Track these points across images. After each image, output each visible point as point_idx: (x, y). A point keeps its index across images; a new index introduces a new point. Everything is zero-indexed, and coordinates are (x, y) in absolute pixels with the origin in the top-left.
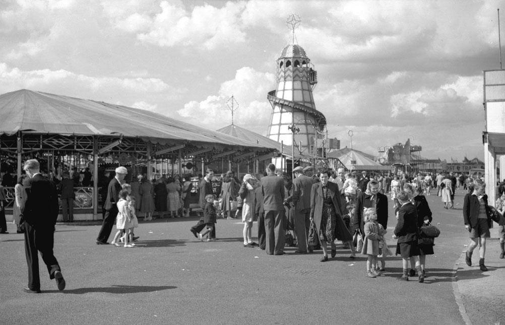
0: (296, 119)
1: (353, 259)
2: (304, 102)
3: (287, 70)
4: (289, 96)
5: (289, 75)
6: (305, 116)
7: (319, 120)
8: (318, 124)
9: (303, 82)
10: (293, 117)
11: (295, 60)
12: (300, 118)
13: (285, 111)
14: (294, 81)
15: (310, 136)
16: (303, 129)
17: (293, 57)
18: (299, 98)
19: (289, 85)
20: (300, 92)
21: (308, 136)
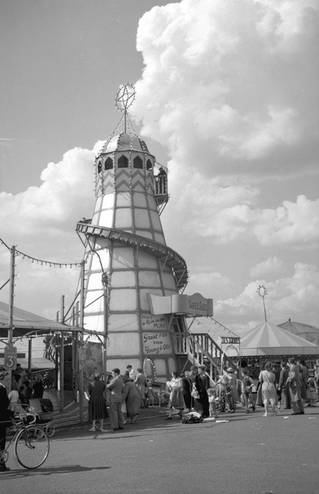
0: (117, 260)
1: (307, 333)
2: (135, 228)
3: (107, 176)
4: (105, 221)
5: (109, 184)
6: (134, 254)
7: (173, 267)
8: (163, 267)
9: (136, 195)
10: (111, 256)
11: (119, 155)
12: (125, 258)
13: (100, 247)
14: (117, 193)
15: (143, 292)
16: (129, 278)
17: (117, 151)
18: (125, 221)
19: (109, 200)
20: (129, 211)
21: (138, 292)
